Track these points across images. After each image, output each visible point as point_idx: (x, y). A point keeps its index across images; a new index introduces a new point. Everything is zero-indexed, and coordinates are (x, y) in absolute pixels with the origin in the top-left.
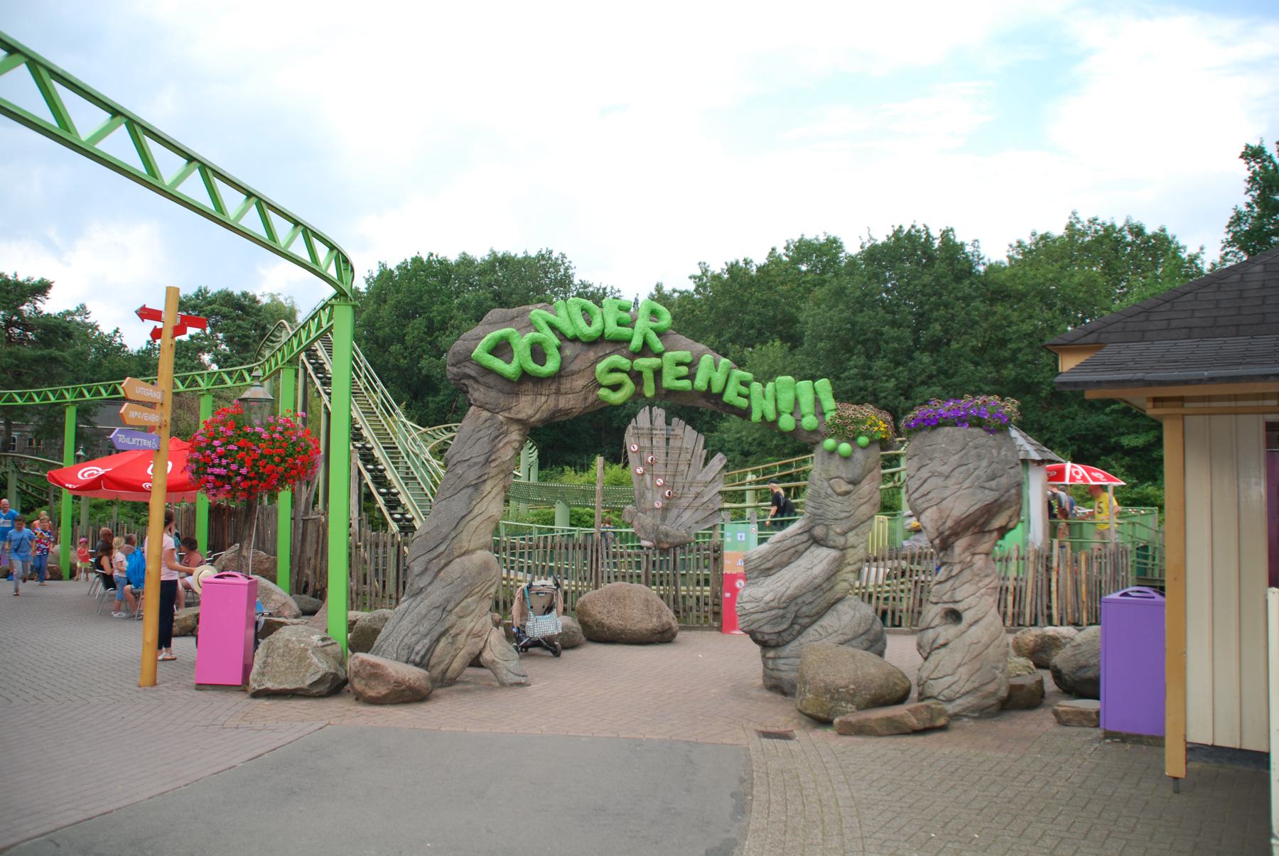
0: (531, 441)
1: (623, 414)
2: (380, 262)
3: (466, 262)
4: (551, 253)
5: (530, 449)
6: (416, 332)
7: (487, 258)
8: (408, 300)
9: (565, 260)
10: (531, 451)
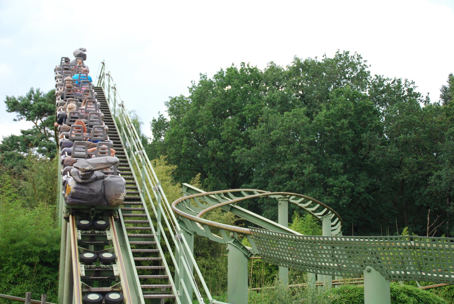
0: (333, 212)
1: (425, 193)
2: (201, 74)
3: (273, 69)
4: (347, 53)
5: (333, 220)
6: (230, 128)
7: (291, 65)
8: (224, 102)
9: (361, 61)
10: (334, 223)
